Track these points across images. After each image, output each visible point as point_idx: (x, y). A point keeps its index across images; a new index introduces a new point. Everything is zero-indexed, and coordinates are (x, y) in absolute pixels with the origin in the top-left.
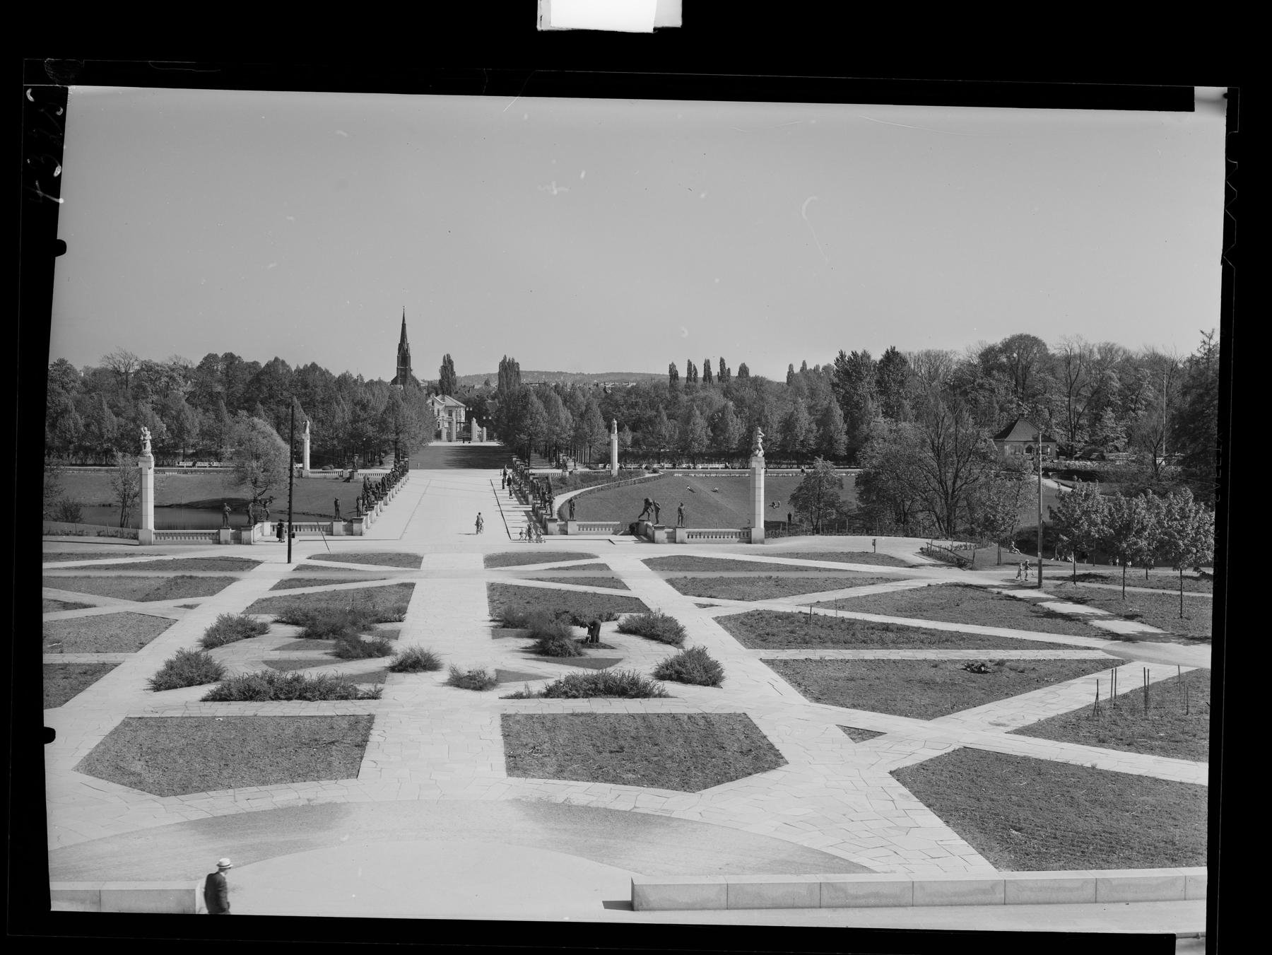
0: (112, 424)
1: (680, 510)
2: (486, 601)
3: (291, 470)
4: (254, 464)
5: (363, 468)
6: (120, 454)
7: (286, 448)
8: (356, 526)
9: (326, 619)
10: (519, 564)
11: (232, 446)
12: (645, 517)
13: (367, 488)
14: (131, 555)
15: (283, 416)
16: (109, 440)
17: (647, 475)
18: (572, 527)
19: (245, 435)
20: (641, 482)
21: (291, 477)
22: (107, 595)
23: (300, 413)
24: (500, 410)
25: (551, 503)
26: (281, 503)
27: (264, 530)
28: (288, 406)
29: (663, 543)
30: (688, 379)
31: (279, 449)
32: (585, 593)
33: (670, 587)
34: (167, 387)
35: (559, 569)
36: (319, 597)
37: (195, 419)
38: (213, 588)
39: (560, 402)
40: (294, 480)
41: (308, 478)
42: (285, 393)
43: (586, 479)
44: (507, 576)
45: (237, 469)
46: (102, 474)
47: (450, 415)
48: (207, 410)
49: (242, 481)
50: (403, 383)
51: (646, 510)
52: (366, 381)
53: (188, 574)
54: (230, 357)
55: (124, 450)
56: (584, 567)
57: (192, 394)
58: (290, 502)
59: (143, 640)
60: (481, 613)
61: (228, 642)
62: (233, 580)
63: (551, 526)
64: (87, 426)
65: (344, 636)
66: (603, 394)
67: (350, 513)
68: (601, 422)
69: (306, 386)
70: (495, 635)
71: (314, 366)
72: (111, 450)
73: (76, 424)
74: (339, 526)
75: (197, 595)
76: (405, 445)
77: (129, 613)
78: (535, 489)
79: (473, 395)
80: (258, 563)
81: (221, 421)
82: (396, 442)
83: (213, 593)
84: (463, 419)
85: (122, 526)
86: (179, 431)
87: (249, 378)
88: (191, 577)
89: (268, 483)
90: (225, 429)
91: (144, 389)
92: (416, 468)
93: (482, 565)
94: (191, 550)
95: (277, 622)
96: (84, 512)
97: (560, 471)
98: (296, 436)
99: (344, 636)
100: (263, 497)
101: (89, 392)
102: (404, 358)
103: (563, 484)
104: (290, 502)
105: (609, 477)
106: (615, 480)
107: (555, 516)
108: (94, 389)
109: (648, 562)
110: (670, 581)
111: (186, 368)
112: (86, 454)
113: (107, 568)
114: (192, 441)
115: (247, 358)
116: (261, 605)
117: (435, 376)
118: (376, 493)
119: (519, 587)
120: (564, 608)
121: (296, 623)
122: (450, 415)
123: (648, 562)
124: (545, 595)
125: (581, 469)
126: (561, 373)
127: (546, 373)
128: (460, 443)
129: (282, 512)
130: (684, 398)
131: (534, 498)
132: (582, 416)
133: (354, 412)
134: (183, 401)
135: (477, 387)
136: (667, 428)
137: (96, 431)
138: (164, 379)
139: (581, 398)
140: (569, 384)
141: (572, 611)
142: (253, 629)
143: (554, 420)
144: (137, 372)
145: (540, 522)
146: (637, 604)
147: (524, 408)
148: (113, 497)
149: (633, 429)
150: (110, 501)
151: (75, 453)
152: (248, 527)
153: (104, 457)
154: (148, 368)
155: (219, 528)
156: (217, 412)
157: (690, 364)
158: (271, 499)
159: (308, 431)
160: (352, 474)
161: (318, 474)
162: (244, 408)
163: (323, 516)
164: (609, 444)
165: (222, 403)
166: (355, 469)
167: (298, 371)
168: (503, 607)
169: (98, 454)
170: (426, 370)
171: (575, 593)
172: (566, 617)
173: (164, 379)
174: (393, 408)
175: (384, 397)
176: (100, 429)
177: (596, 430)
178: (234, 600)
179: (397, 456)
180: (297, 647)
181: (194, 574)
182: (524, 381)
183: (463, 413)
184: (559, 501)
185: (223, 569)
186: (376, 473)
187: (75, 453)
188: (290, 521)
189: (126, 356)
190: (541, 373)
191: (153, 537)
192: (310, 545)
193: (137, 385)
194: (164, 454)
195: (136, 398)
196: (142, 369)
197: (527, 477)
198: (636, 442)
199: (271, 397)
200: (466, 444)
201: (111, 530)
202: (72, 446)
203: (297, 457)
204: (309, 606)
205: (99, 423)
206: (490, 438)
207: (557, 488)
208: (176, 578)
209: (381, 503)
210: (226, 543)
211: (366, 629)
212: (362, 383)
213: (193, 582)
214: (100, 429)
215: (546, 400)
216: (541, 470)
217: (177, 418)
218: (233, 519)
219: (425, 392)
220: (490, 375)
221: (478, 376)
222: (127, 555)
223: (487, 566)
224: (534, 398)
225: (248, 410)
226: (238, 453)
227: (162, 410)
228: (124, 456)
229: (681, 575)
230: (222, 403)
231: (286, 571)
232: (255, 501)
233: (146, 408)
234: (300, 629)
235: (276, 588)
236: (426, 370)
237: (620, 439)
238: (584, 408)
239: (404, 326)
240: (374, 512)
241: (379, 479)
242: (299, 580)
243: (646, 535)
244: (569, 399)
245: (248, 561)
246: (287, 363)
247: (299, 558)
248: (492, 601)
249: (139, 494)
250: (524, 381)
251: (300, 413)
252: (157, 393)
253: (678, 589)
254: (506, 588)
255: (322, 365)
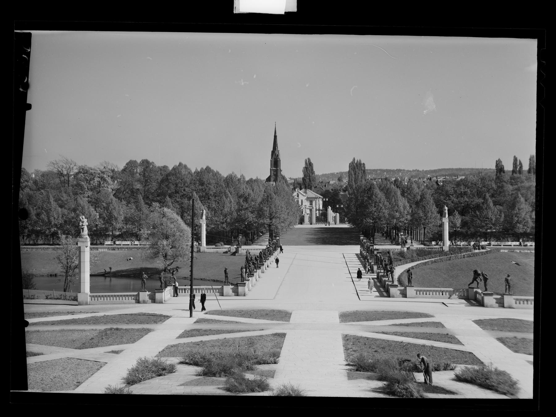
0: (57, 214)
1: (507, 280)
2: (342, 349)
3: (192, 247)
4: (165, 242)
5: (246, 244)
6: (64, 236)
7: (188, 230)
8: (240, 289)
9: (219, 361)
10: (367, 320)
11: (148, 229)
12: (475, 285)
14: (73, 313)
15: (186, 207)
16: (56, 225)
18: (410, 291)
19: (157, 221)
20: (469, 256)
22: (53, 345)
23: (198, 204)
24: (350, 200)
25: (392, 272)
26: (185, 272)
28: (189, 198)
29: (491, 307)
30: (514, 172)
32: (424, 346)
33: (501, 345)
35: (401, 325)
36: (213, 344)
37: (121, 210)
38: (134, 337)
39: (399, 193)
40: (194, 254)
41: (204, 252)
42: (187, 189)
43: (421, 254)
44: (358, 329)
45: (153, 246)
46: (50, 251)
47: (311, 204)
48: (129, 203)
49: (156, 255)
50: (275, 180)
51: (475, 279)
52: (247, 179)
54: (146, 163)
56: (422, 325)
57: (118, 190)
58: (191, 271)
59: (80, 380)
60: (338, 358)
61: (145, 380)
62: (149, 331)
63: (392, 290)
65: (231, 374)
66: (436, 186)
67: (234, 280)
68: (434, 209)
69: (202, 184)
70: (350, 377)
74: (228, 289)
75: (121, 343)
76: (277, 228)
77: (69, 359)
78: (378, 261)
79: (330, 188)
80: (168, 317)
81: (140, 210)
82: (270, 226)
83: (134, 341)
84: (321, 207)
86: (109, 219)
87: (160, 178)
88: (117, 329)
89: (175, 257)
91: (82, 188)
93: (338, 320)
95: (182, 363)
97: (399, 247)
98: (196, 221)
99: (231, 374)
100: (171, 267)
101: (39, 189)
102: (276, 162)
103: (402, 257)
104: (191, 271)
105: (441, 252)
106: (446, 254)
107: (396, 283)
108: (44, 187)
109: (479, 322)
110: (501, 340)
111: (113, 171)
112: (37, 236)
113: (53, 323)
114: (118, 226)
115: (159, 163)
116: (170, 350)
117: (299, 175)
118: (254, 264)
119: (368, 339)
120: (405, 357)
121: (196, 364)
122: (311, 204)
123: (479, 322)
125: (416, 246)
126: (399, 171)
127: (388, 171)
129: (185, 278)
130: (509, 188)
131: (378, 268)
132: (417, 203)
133: (238, 203)
135: (332, 182)
136: (494, 212)
138: (97, 179)
139: (416, 190)
140: (406, 179)
142: (164, 369)
143: (394, 207)
144: (77, 174)
147: (370, 198)
148: (58, 269)
149: (462, 213)
151: (29, 236)
152: (161, 290)
154: (84, 171)
156: (137, 202)
157: (515, 159)
158: (177, 268)
159: (204, 217)
160: (237, 251)
161: (211, 249)
163: (216, 281)
164: (442, 225)
165: (140, 197)
166: (239, 245)
167: (197, 173)
168: (356, 355)
169: (47, 236)
170: (292, 170)
171: (415, 345)
175: (260, 191)
176: (49, 218)
178: (149, 347)
179: (271, 236)
180: (197, 383)
181: (120, 326)
182: (369, 177)
183: (321, 202)
184: (399, 270)
185: (141, 323)
186: (255, 249)
187: (29, 236)
188: (191, 285)
189: (67, 162)
190: (383, 171)
193: (76, 184)
194: (97, 236)
195: (76, 194)
197: (372, 252)
198: (464, 224)
199: (177, 192)
202: (26, 231)
203: (196, 237)
204: (206, 351)
205: (48, 214)
206: (342, 221)
208: (106, 330)
209: (259, 271)
210: (144, 302)
211: (249, 369)
212: (244, 181)
213: (119, 332)
214: (49, 218)
215: (388, 193)
218: (149, 283)
219: (292, 187)
220: (342, 173)
221: (332, 174)
222: (68, 313)
224: (377, 191)
226: (152, 235)
227: (95, 203)
228: (67, 238)
229: (511, 335)
230: (140, 197)
232: (165, 270)
233: (83, 201)
234: (199, 369)
235: (181, 337)
236: (292, 170)
237: (450, 222)
238: (419, 197)
239: (275, 137)
240: (254, 278)
241: (257, 253)
242: (198, 330)
243: (476, 299)
244: (406, 191)
245: (161, 316)
246: (189, 166)
248: (346, 349)
249: (78, 266)
250: (369, 177)
251: (198, 204)
252: (92, 190)
253: (509, 347)
254: (357, 340)
255: (214, 168)
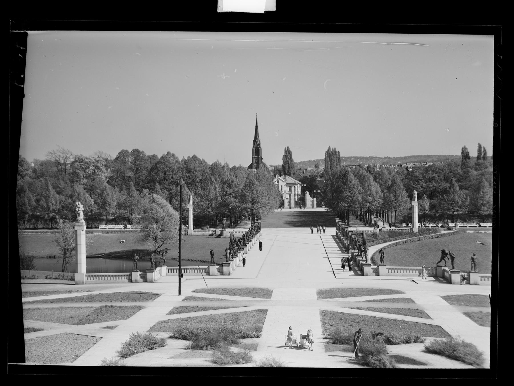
0: (55, 200)
1: (473, 259)
3: (180, 230)
4: (155, 226)
6: (61, 221)
7: (176, 214)
10: (343, 297)
11: (139, 214)
12: (442, 263)
13: (232, 242)
14: (70, 292)
15: (174, 192)
16: (54, 211)
17: (443, 232)
18: (383, 269)
19: (148, 206)
20: (437, 237)
21: (180, 235)
22: (52, 321)
23: (186, 190)
24: (326, 185)
25: (366, 252)
27: (161, 273)
28: (177, 185)
30: (478, 158)
31: (170, 216)
32: (395, 320)
33: (468, 319)
34: (94, 173)
35: (374, 301)
36: (200, 320)
37: (114, 196)
38: (127, 313)
39: (372, 178)
40: (182, 237)
46: (49, 235)
49: (146, 238)
50: (257, 168)
51: (443, 258)
52: (231, 166)
53: (109, 304)
54: (136, 152)
55: (64, 218)
56: (393, 300)
57: (111, 178)
58: (180, 252)
59: (78, 353)
61: (137, 353)
62: (141, 308)
63: (366, 269)
64: (38, 201)
66: (406, 172)
67: (219, 260)
68: (404, 193)
69: (189, 171)
71: (195, 158)
72: (55, 218)
73: (29, 200)
74: (214, 269)
75: (115, 319)
76: (259, 212)
77: (67, 334)
79: (308, 174)
80: (158, 295)
81: (131, 196)
83: (127, 318)
84: (300, 193)
85: (63, 271)
86: (103, 204)
87: (150, 166)
88: (112, 306)
89: (164, 239)
90: (135, 202)
91: (78, 175)
92: (264, 228)
93: (316, 297)
94: (112, 287)
95: (171, 337)
96: (36, 262)
97: (372, 229)
101: (38, 177)
102: (257, 151)
104: (180, 252)
105: (411, 234)
106: (415, 235)
107: (369, 262)
108: (42, 175)
109: (447, 298)
110: (467, 314)
111: (106, 160)
112: (37, 221)
113: (52, 301)
114: (112, 211)
115: (148, 152)
116: (160, 326)
117: (280, 162)
118: (238, 245)
119: (343, 314)
120: (379, 331)
121: (185, 338)
123: (447, 298)
124: (364, 320)
126: (372, 158)
127: (361, 158)
128: (298, 210)
129: (174, 259)
132: (388, 188)
134: (105, 183)
135: (309, 169)
137: (45, 205)
138: (92, 168)
139: (387, 176)
140: (378, 165)
141: (386, 333)
142: (155, 343)
143: (367, 191)
144: (73, 163)
145: (358, 266)
146: (439, 331)
147: (344, 183)
148: (57, 251)
150: (55, 254)
151: (29, 221)
152: (151, 270)
153: (51, 223)
154: (80, 160)
155: (131, 271)
156: (128, 189)
158: (166, 250)
159: (191, 202)
161: (198, 232)
162: (145, 188)
163: (202, 262)
164: (411, 208)
167: (185, 161)
168: (333, 329)
169: (46, 220)
170: (273, 158)
171: (387, 320)
172: (381, 338)
173: (92, 168)
174: (250, 185)
175: (243, 178)
177: (400, 198)
180: (186, 356)
181: (114, 304)
183: (300, 188)
184: (372, 250)
185: (134, 301)
186: (239, 232)
191: (85, 279)
192: (194, 281)
193: (69, 174)
194: (93, 221)
195: (72, 181)
196: (75, 161)
198: (432, 207)
199: (165, 179)
200: (302, 210)
201: (55, 274)
202: (27, 216)
203: (184, 221)
204: (194, 327)
206: (319, 205)
207: (370, 241)
208: (101, 307)
210: (136, 281)
211: (234, 343)
212: (228, 169)
214: (47, 205)
216: (357, 228)
217: (101, 195)
218: (140, 264)
219: (272, 174)
220: (318, 161)
222: (66, 292)
223: (319, 298)
224: (351, 176)
225: (150, 189)
226: (143, 219)
227: (90, 190)
228: (64, 222)
231: (177, 301)
232: (155, 252)
234: (188, 343)
235: (170, 313)
236: (273, 158)
237: (419, 205)
238: (390, 183)
239: (257, 127)
241: (241, 235)
242: (186, 307)
243: (443, 277)
244: (378, 177)
246: (176, 155)
247: (187, 291)
249: (75, 249)
250: (344, 164)
251: (186, 190)
252: (87, 177)
253: (475, 321)
254: (334, 315)
255: (200, 156)
